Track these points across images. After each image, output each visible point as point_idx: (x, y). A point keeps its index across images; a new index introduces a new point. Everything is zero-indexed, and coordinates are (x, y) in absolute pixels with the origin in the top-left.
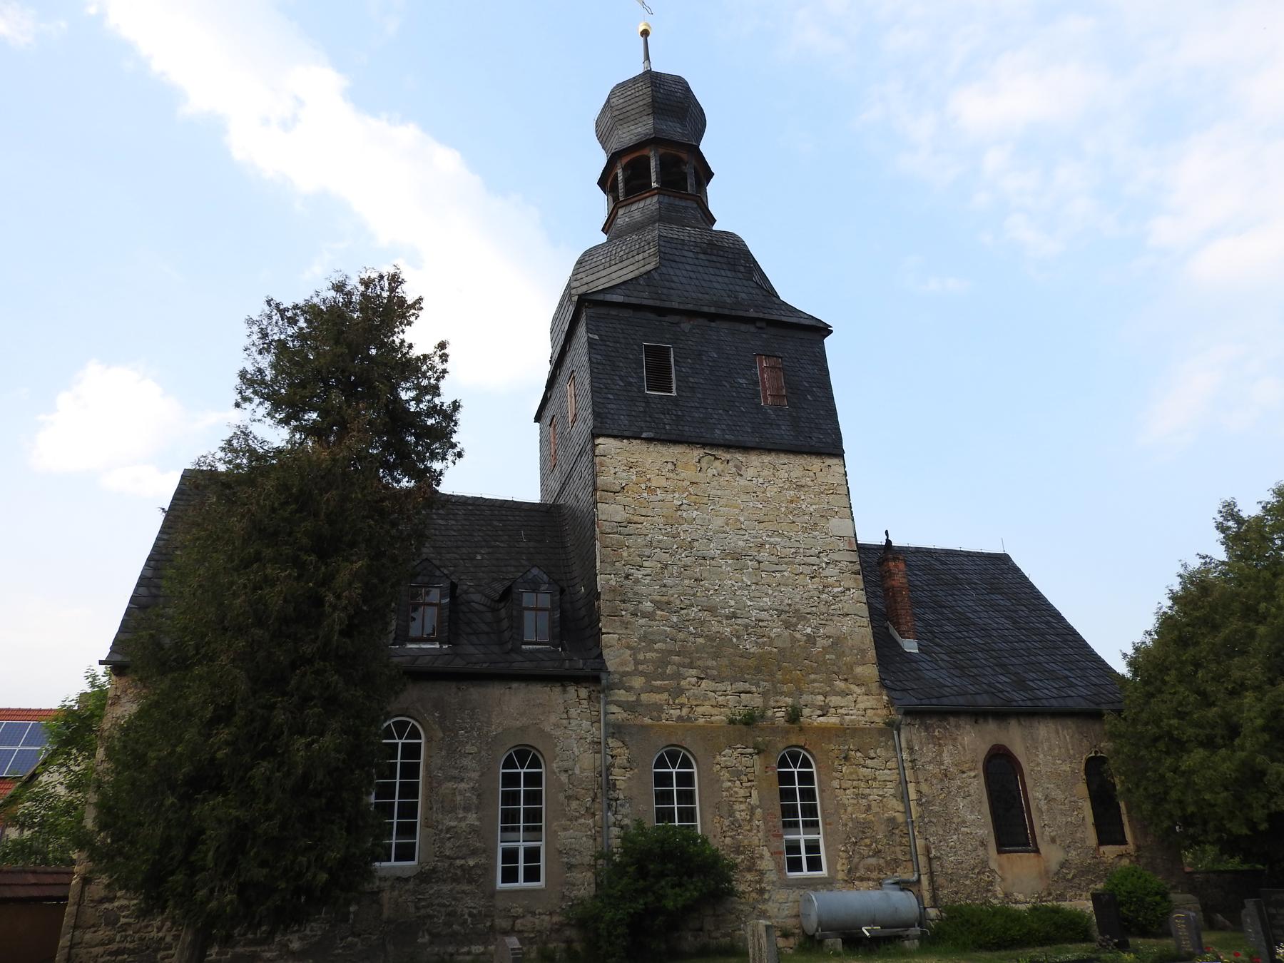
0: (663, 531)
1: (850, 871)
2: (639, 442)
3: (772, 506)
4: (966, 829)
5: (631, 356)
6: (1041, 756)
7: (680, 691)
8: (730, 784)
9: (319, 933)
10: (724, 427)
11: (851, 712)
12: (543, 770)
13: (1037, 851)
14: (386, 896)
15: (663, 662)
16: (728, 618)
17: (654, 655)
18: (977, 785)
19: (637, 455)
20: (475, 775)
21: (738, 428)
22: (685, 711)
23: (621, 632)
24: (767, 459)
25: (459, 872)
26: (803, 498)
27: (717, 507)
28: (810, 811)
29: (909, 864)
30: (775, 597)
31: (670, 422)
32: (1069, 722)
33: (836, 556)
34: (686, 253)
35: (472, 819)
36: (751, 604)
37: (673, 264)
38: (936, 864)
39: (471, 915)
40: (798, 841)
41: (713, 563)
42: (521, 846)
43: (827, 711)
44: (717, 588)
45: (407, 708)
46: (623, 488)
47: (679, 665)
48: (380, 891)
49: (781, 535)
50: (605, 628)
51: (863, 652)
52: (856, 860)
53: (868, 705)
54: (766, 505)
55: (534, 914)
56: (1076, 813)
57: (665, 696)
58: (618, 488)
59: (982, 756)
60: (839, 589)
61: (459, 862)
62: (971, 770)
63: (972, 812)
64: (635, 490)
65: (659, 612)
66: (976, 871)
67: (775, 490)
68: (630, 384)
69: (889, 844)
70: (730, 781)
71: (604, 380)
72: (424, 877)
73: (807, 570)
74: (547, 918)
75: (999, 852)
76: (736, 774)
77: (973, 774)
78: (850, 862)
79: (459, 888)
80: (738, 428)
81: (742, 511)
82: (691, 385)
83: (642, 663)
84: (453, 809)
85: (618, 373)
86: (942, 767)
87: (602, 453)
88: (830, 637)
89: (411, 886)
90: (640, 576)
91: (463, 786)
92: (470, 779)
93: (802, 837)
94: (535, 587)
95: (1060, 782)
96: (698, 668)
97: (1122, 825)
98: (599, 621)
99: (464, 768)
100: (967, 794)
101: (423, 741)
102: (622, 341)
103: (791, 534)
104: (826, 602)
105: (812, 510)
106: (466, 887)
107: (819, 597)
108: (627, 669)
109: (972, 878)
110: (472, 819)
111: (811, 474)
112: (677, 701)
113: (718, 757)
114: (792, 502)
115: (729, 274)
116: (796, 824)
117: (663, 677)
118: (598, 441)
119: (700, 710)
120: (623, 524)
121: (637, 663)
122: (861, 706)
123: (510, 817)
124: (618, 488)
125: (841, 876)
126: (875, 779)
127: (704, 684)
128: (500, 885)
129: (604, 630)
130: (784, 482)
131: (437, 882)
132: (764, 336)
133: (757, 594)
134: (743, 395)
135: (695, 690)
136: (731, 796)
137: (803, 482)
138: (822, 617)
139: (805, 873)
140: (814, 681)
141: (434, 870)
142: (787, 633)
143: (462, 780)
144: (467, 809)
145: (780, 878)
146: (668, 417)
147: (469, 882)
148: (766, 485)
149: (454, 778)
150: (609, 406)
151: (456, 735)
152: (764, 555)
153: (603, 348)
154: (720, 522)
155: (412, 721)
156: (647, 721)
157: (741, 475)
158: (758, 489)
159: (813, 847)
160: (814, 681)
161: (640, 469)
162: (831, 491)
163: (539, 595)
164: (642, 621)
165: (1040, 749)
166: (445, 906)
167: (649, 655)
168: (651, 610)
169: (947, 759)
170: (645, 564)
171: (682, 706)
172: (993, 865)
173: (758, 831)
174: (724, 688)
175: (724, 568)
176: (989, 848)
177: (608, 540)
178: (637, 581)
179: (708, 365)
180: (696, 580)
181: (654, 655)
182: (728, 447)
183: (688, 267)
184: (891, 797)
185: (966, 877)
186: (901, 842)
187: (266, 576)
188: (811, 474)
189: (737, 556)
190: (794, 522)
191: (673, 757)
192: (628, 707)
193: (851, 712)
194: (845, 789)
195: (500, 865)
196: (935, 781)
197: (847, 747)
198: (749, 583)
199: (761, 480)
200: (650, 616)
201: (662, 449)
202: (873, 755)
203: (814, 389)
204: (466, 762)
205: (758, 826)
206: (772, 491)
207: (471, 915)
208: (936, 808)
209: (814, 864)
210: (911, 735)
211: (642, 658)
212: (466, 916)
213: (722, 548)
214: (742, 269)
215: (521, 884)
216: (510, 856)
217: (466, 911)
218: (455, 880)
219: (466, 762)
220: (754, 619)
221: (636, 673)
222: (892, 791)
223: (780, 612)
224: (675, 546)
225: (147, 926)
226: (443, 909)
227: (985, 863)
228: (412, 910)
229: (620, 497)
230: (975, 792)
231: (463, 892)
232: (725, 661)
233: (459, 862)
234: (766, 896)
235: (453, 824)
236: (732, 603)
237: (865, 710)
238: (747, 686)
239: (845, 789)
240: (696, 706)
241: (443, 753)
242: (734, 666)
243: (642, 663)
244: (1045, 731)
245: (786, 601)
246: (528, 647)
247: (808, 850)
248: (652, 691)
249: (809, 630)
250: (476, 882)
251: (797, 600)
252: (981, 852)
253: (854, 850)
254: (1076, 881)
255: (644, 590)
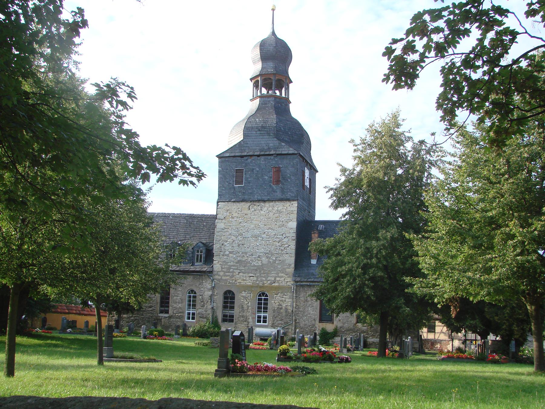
14: (163, 320)
17: (227, 266)
19: (230, 207)
20: (181, 295)
24: (271, 204)
28: (266, 308)
35: (180, 305)
48: (162, 319)
53: (288, 280)
58: (223, 218)
68: (230, 183)
72: (170, 317)
73: (278, 240)
75: (319, 322)
76: (245, 298)
83: (224, 268)
84: (176, 303)
89: (167, 319)
91: (178, 298)
93: (262, 315)
97: (133, 341)
102: (229, 169)
106: (178, 320)
110: (180, 305)
111: (285, 207)
114: (277, 218)
117: (229, 272)
119: (238, 281)
122: (286, 281)
123: (189, 305)
124: (223, 218)
126: (285, 301)
128: (186, 320)
133: (260, 248)
135: (238, 276)
139: (262, 323)
141: (172, 316)
144: (179, 303)
147: (179, 319)
152: (264, 236)
154: (253, 226)
159: (265, 317)
164: (225, 257)
171: (233, 280)
178: (225, 245)
181: (227, 266)
182: (259, 201)
183: (253, 137)
185: (307, 328)
187: (531, 102)
188: (285, 207)
189: (256, 237)
195: (186, 316)
199: (268, 211)
200: (228, 255)
201: (238, 204)
215: (191, 320)
216: (189, 314)
218: (177, 318)
221: (222, 271)
223: (266, 253)
227: (314, 325)
229: (224, 221)
252: (313, 322)
254: (345, 332)
255: (227, 248)
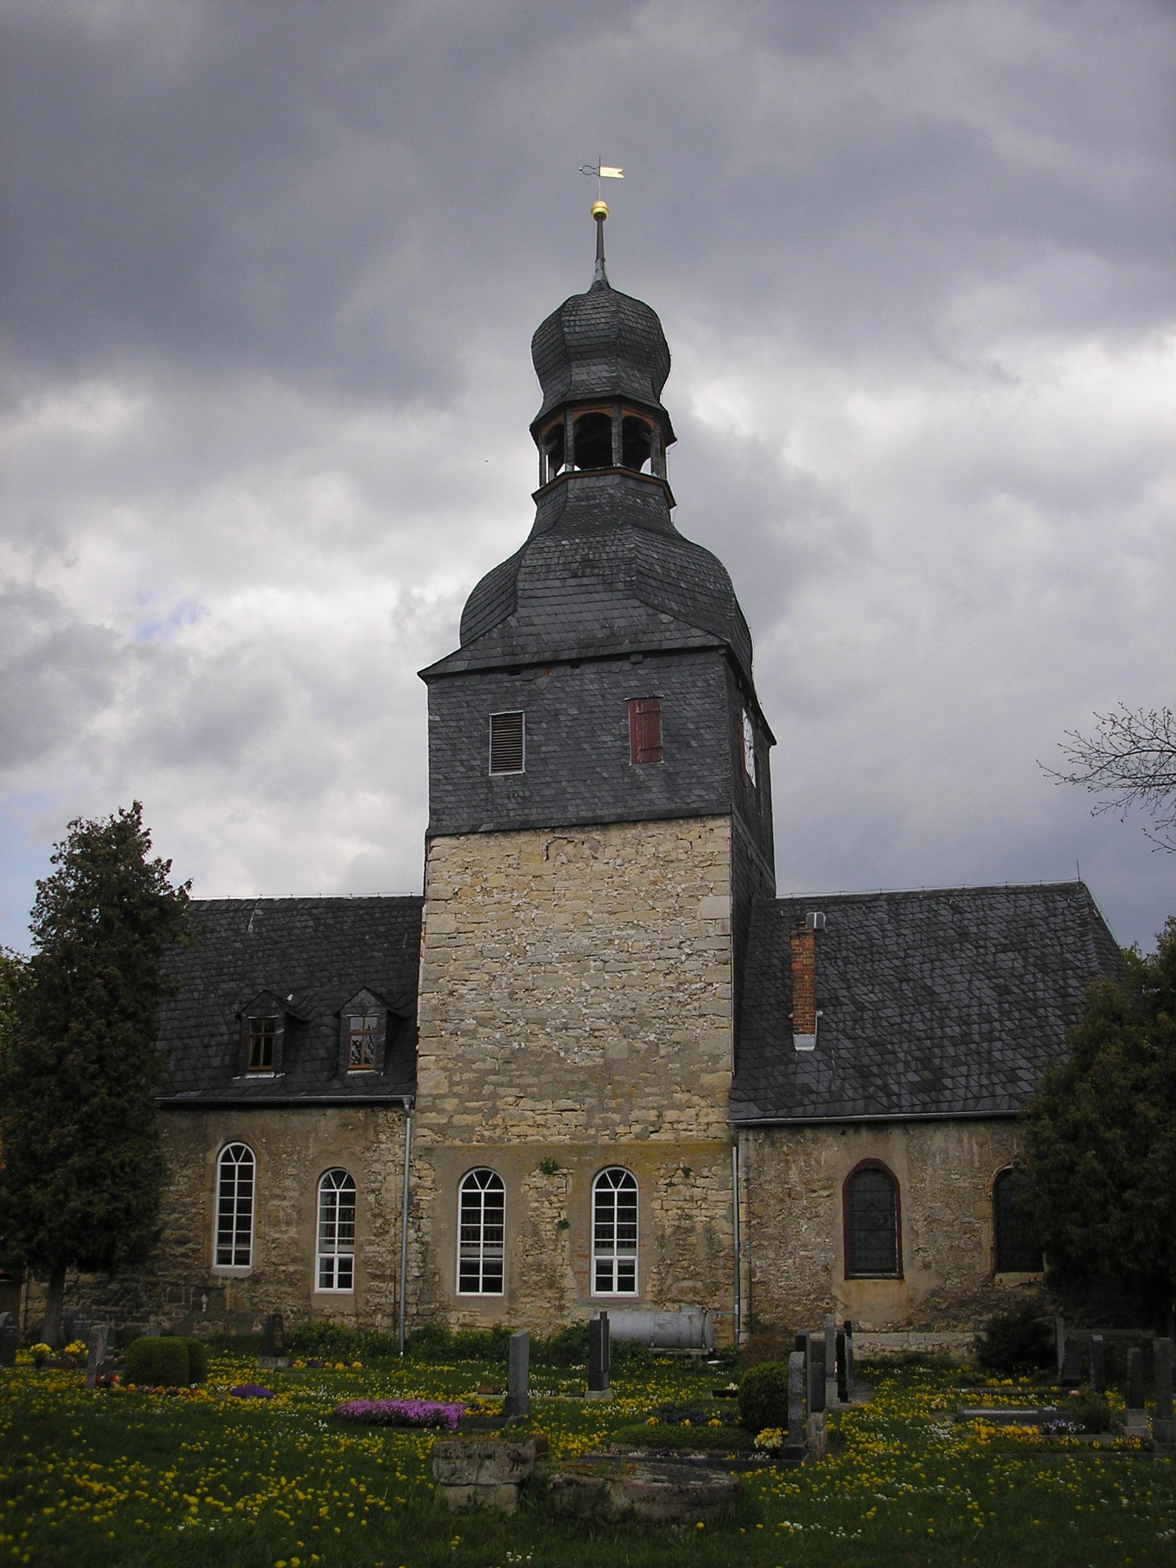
0: (496, 938)
1: (660, 1292)
2: (477, 836)
3: (629, 892)
4: (806, 1253)
5: (475, 734)
6: (930, 1171)
7: (494, 1112)
8: (536, 1204)
9: (182, 1316)
10: (579, 801)
11: (690, 1127)
12: (254, 1164)
13: (901, 1277)
14: (228, 1291)
15: (479, 1082)
16: (557, 1029)
17: (471, 1075)
18: (834, 1207)
21: (596, 800)
22: (498, 1132)
23: (438, 1053)
24: (631, 833)
25: (282, 1276)
26: (670, 876)
27: (562, 902)
29: (731, 1289)
30: (618, 1001)
31: (516, 806)
32: (982, 1129)
33: (699, 945)
34: (549, 583)
35: (293, 1232)
36: (587, 1011)
37: (534, 602)
38: (759, 1290)
39: (292, 1312)
40: (611, 1262)
41: (549, 967)
42: (336, 1257)
43: (660, 1128)
44: (549, 996)
45: (240, 1135)
46: (456, 893)
47: (497, 1085)
49: (636, 926)
50: (423, 1050)
51: (715, 1058)
52: (669, 1282)
53: (712, 1118)
54: (622, 891)
55: (343, 1315)
56: (968, 1235)
57: (478, 1118)
58: (450, 895)
59: (844, 1174)
60: (698, 986)
61: (282, 1268)
62: (824, 1189)
63: (818, 1234)
64: (468, 894)
65: (480, 1029)
66: (812, 1297)
67: (636, 871)
68: (472, 768)
69: (710, 1267)
70: (538, 1201)
71: (444, 770)
72: (256, 1279)
73: (662, 965)
74: (354, 1319)
75: (847, 1277)
77: (825, 1193)
78: (662, 1284)
79: (283, 1289)
80: (596, 800)
81: (592, 902)
82: (542, 756)
83: (458, 1084)
84: (277, 1223)
85: (458, 757)
86: (786, 1186)
87: (436, 857)
88: (678, 1043)
89: (246, 1285)
90: (465, 992)
91: (285, 1203)
92: (291, 1197)
93: (615, 1257)
94: (363, 1012)
95: (951, 1200)
96: (518, 1085)
98: (417, 1043)
99: (286, 1189)
100: (814, 1214)
101: (254, 1164)
102: (467, 716)
103: (648, 923)
104: (680, 1002)
105: (679, 890)
106: (289, 1290)
107: (671, 997)
108: (441, 1092)
109: (805, 1304)
110: (293, 1232)
111: (686, 844)
112: (490, 1122)
113: (526, 1177)
114: (655, 883)
115: (604, 596)
116: (611, 1244)
118: (433, 843)
119: (515, 1130)
120: (451, 935)
121: (452, 1084)
122: (703, 1120)
124: (450, 895)
125: (649, 1297)
127: (522, 1102)
129: (420, 1053)
130: (649, 859)
131: (265, 1283)
132: (641, 672)
133: (596, 999)
134: (607, 756)
136: (538, 1216)
137: (673, 856)
138: (670, 1020)
140: (649, 1095)
141: (262, 1274)
142: (625, 1042)
143: (285, 1198)
144: (288, 1224)
145: (581, 1297)
146: (513, 801)
148: (626, 865)
149: (278, 1197)
150: (447, 799)
151: (280, 1157)
153: (444, 730)
155: (246, 1147)
156: (458, 1143)
157: (596, 858)
158: (614, 873)
160: (649, 1095)
161: (476, 869)
162: (709, 863)
163: (367, 1019)
164: (461, 1040)
165: (929, 1162)
166: (271, 1303)
167: (466, 1076)
168: (472, 1027)
169: (794, 1176)
170: (472, 977)
171: (495, 1127)
172: (836, 1291)
173: (563, 1251)
174: (544, 1107)
175: (560, 972)
176: (834, 1274)
177: (434, 954)
178: (462, 996)
179: (566, 726)
180: (527, 990)
181: (471, 1075)
182: (583, 825)
183: (553, 601)
184: (721, 1219)
185: (798, 1302)
186: (725, 1265)
189: (579, 958)
190: (654, 908)
191: (483, 1176)
192: (440, 1130)
193: (690, 1127)
194: (667, 1211)
196: (772, 1202)
197: (676, 1166)
198: (588, 988)
199: (619, 861)
200: (471, 1034)
202: (705, 1173)
203: (702, 731)
204: (287, 1183)
205: (563, 1246)
206: (632, 872)
207: (292, 1312)
208: (770, 1231)
209: (626, 1285)
210: (747, 1147)
211: (458, 1079)
212: (289, 1313)
213: (561, 950)
214: (621, 586)
217: (288, 1308)
218: (279, 1282)
219: (287, 1183)
220: (588, 1029)
221: (451, 1094)
222: (724, 1212)
223: (617, 1019)
224: (509, 954)
225: (70, 1301)
226: (271, 1306)
228: (247, 1305)
230: (825, 1213)
231: (286, 1293)
232: (545, 1078)
233: (282, 1268)
234: (565, 1313)
235: (277, 1236)
236: (565, 1012)
237: (708, 1124)
238: (569, 1104)
239: (667, 1211)
240: (512, 1126)
241: (269, 1174)
242: (558, 1082)
243: (458, 1084)
244: (939, 1140)
245: (630, 1005)
246: (353, 1072)
247: (621, 1270)
248: (464, 1113)
249: (652, 1037)
250: (296, 1284)
251: (644, 1003)
252: (823, 1278)
253: (668, 1272)
254: (953, 1311)
